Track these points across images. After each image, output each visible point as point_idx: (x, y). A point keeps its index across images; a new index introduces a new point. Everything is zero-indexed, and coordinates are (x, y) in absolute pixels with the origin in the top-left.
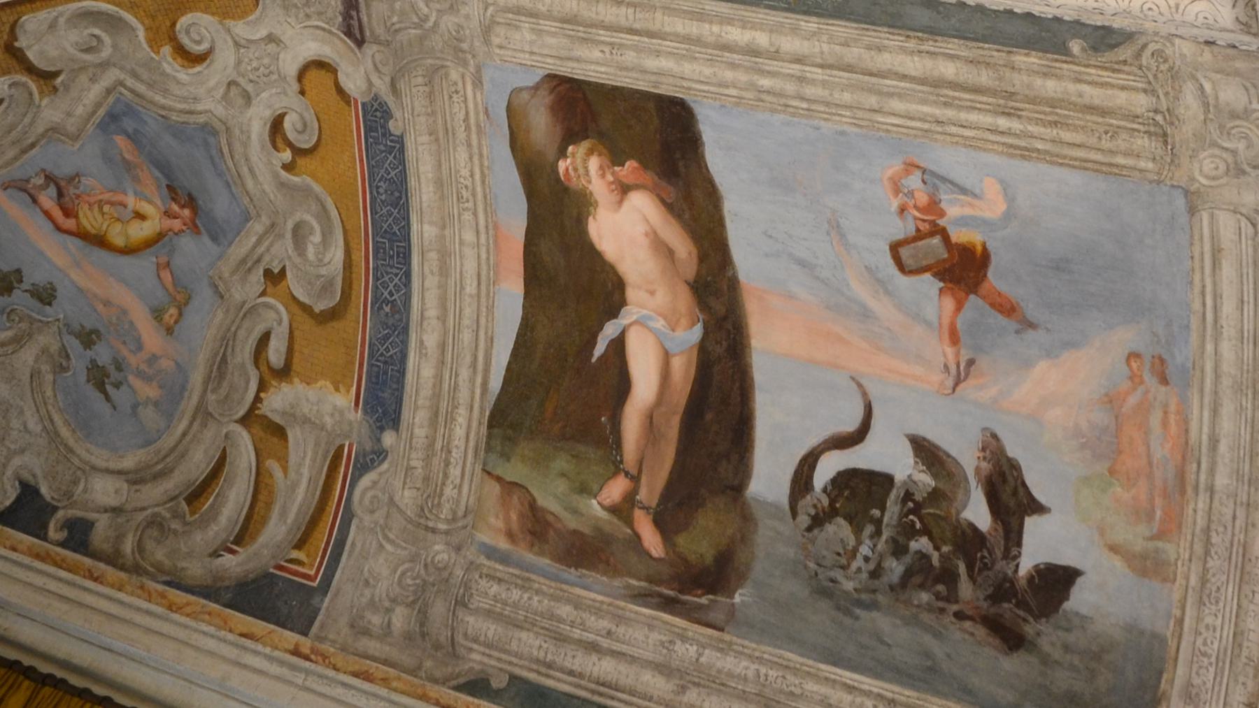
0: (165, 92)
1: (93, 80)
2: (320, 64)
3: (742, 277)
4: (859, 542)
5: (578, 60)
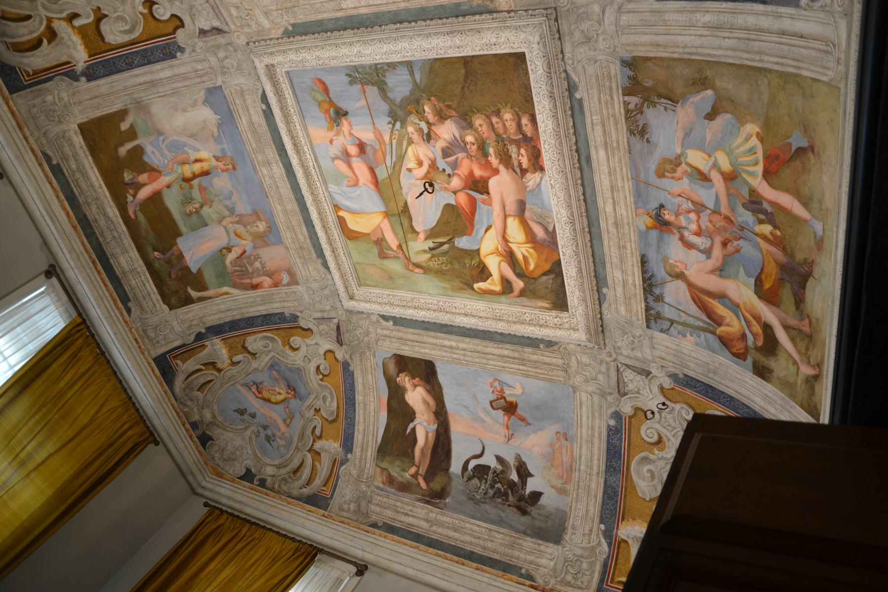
0: (287, 359)
1: (266, 355)
2: (330, 351)
3: (448, 411)
4: (481, 485)
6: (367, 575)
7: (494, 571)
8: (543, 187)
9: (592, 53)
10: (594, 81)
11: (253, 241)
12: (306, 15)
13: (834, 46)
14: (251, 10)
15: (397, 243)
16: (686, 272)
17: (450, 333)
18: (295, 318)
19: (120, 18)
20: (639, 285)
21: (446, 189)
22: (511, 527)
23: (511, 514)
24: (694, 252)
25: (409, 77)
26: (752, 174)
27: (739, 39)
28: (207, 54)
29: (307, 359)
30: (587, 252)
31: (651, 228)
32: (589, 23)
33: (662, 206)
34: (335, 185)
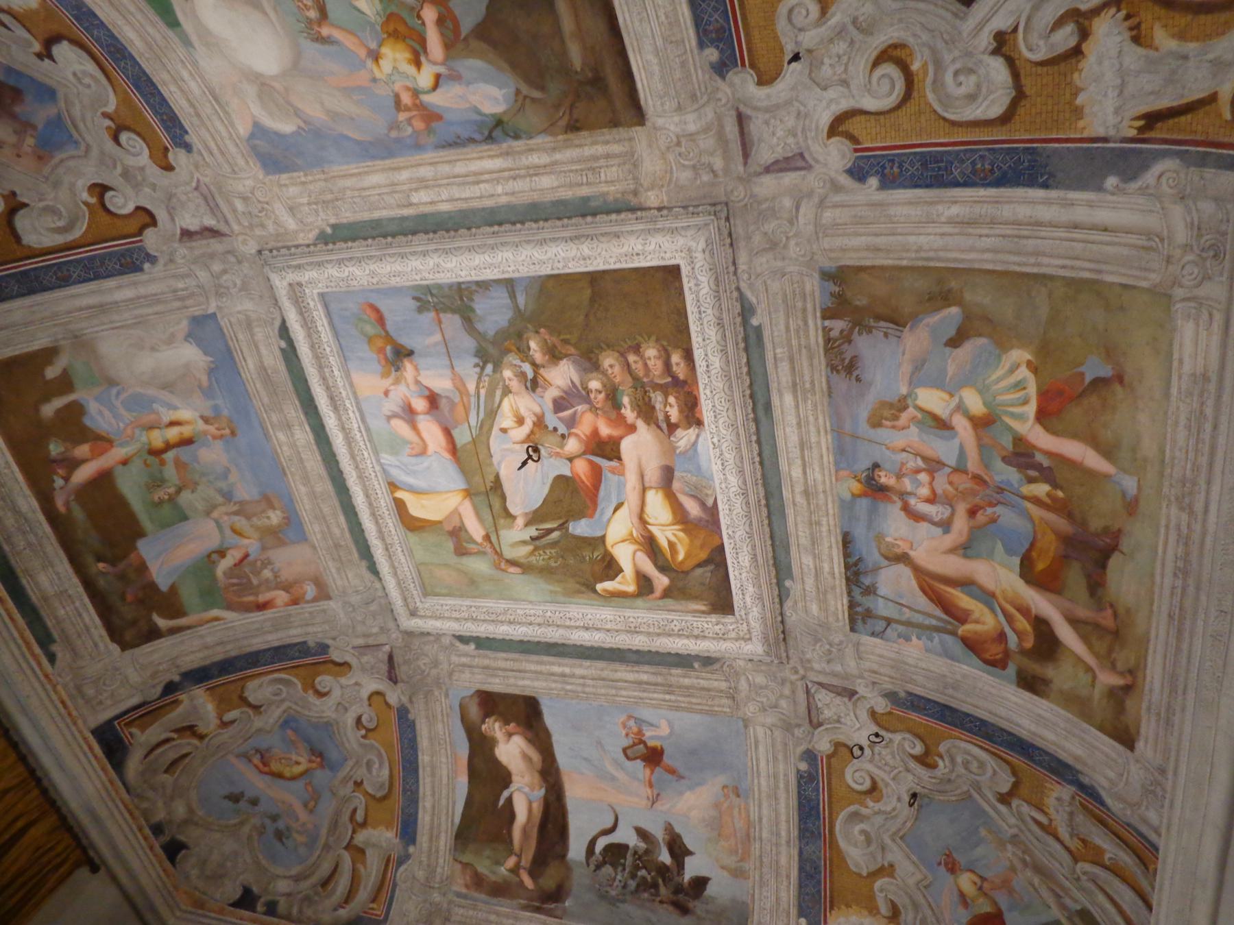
0: (310, 710)
1: (278, 707)
2: (378, 693)
4: (616, 874)
5: (489, 683)
8: (700, 447)
9: (779, 264)
11: (261, 539)
12: (355, 212)
13: (1162, 240)
14: (267, 203)
15: (482, 533)
16: (912, 553)
18: (323, 648)
19: (52, 210)
20: (840, 573)
21: (558, 454)
24: (924, 525)
25: (509, 301)
26: (1021, 417)
27: (1004, 236)
28: (193, 267)
29: (342, 707)
30: (763, 531)
31: (859, 496)
32: (776, 222)
33: (876, 466)
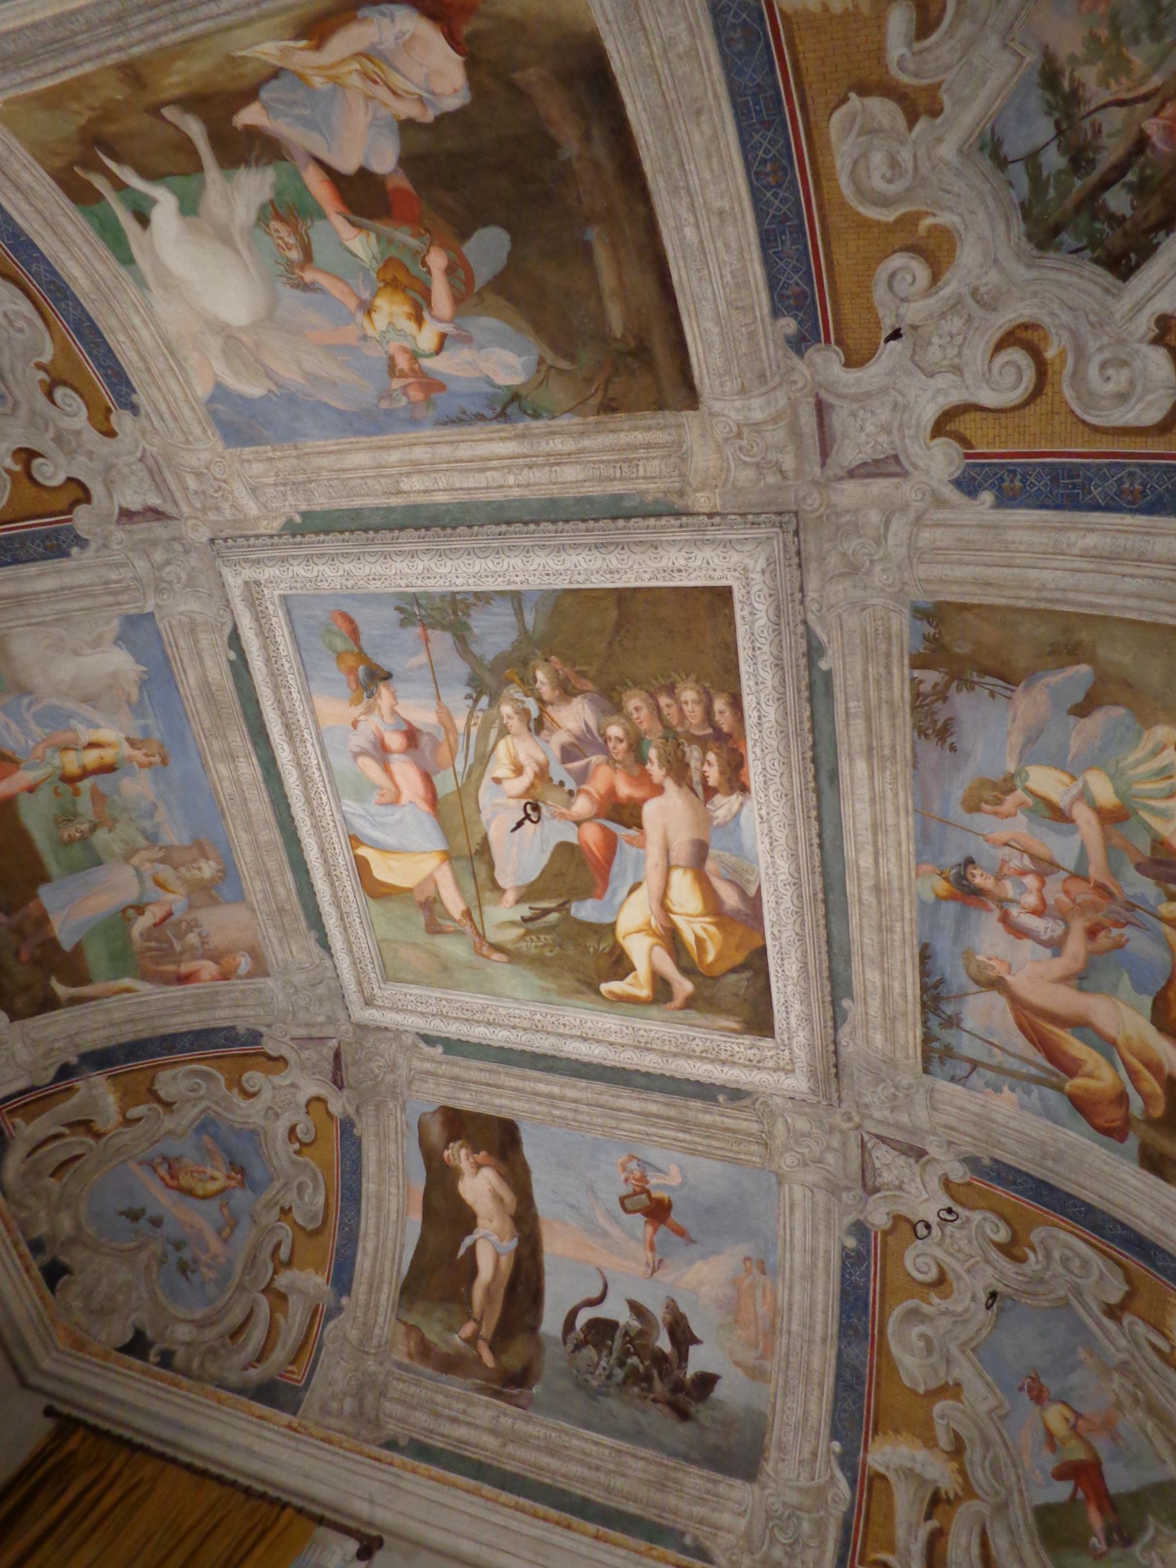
1: (194, 1106)
2: (318, 1099)
3: (540, 1213)
4: (600, 1359)
6: (379, 1557)
7: (632, 1541)
8: (743, 820)
9: (859, 593)
10: (858, 642)
11: (188, 895)
16: (1009, 978)
17: (550, 1069)
18: (256, 1037)
22: (659, 1446)
23: (658, 1419)
24: (1028, 944)
25: (513, 619)
27: (1154, 578)
28: (130, 554)
29: (273, 1113)
31: (945, 898)
33: (970, 861)
34: (356, 800)
